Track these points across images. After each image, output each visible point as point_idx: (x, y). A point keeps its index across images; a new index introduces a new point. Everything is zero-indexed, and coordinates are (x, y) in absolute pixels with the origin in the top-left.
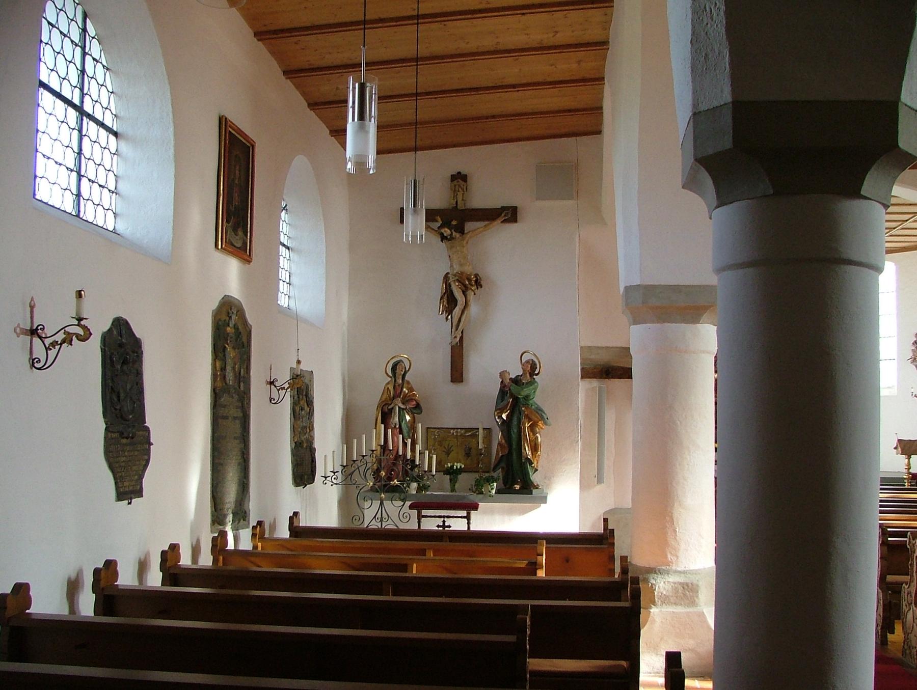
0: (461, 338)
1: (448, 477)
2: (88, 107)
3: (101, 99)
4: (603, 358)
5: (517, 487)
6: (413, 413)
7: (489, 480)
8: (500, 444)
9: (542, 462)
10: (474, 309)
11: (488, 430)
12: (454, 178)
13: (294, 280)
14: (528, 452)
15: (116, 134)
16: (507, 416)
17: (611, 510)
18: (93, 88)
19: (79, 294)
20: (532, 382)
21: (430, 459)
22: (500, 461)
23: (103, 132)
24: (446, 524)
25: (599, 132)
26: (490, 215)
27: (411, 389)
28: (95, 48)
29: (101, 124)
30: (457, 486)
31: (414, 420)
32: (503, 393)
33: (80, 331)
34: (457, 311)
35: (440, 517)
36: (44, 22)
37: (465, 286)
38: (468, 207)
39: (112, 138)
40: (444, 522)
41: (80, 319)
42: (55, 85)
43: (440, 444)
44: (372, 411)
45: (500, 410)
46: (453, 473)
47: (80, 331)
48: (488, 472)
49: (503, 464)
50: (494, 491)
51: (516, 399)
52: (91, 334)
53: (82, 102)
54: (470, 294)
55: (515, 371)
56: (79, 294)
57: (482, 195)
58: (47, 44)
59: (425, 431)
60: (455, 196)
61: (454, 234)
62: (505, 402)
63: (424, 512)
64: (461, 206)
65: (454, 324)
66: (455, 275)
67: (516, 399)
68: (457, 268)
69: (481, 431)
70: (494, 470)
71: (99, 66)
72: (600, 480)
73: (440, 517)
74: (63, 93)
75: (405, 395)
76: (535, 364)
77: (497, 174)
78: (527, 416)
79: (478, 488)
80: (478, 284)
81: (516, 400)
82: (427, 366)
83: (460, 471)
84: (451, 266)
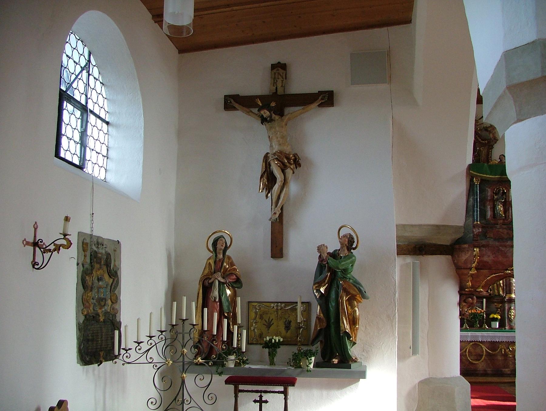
0: (281, 215)
1: (267, 349)
2: (90, 106)
3: (98, 101)
4: (417, 235)
5: (336, 361)
6: (233, 287)
7: (307, 354)
8: (318, 318)
9: (362, 334)
10: (293, 187)
11: (307, 305)
12: (273, 67)
13: (112, 154)
14: (346, 325)
15: (108, 123)
16: (325, 290)
17: (426, 380)
18: (94, 96)
19: (67, 219)
20: (350, 256)
21: (240, 334)
22: (318, 334)
23: (99, 121)
24: (263, 399)
25: (408, 21)
26: (306, 100)
27: (232, 264)
28: (95, 72)
29: (99, 117)
30: (275, 359)
31: (235, 295)
32: (321, 267)
33: (64, 242)
34: (276, 188)
35: (257, 391)
36: (64, 55)
37: (283, 163)
38: (286, 93)
39: (105, 125)
40: (261, 397)
41: (65, 235)
42: (97, 111)
43: (261, 317)
44: (195, 287)
45: (318, 284)
46: (272, 347)
47: (64, 242)
48: (307, 345)
49: (321, 338)
50: (311, 366)
51: (335, 273)
52: (71, 244)
53: (87, 103)
54: (289, 171)
55: (333, 245)
56: (67, 219)
57: (300, 83)
58: (65, 68)
59: (246, 305)
60: (275, 83)
61: (273, 115)
62: (323, 276)
63: (241, 387)
64: (280, 92)
65: (274, 201)
66: (274, 154)
67: (335, 273)
68: (276, 148)
69: (299, 304)
70: (313, 343)
71: (98, 82)
72: (415, 352)
73: (257, 391)
74: (101, 116)
75: (226, 270)
76: (353, 238)
77: (313, 62)
78: (345, 290)
79: (296, 361)
80: (297, 163)
81: (334, 273)
82: (248, 241)
83: (278, 345)
84: (271, 146)
